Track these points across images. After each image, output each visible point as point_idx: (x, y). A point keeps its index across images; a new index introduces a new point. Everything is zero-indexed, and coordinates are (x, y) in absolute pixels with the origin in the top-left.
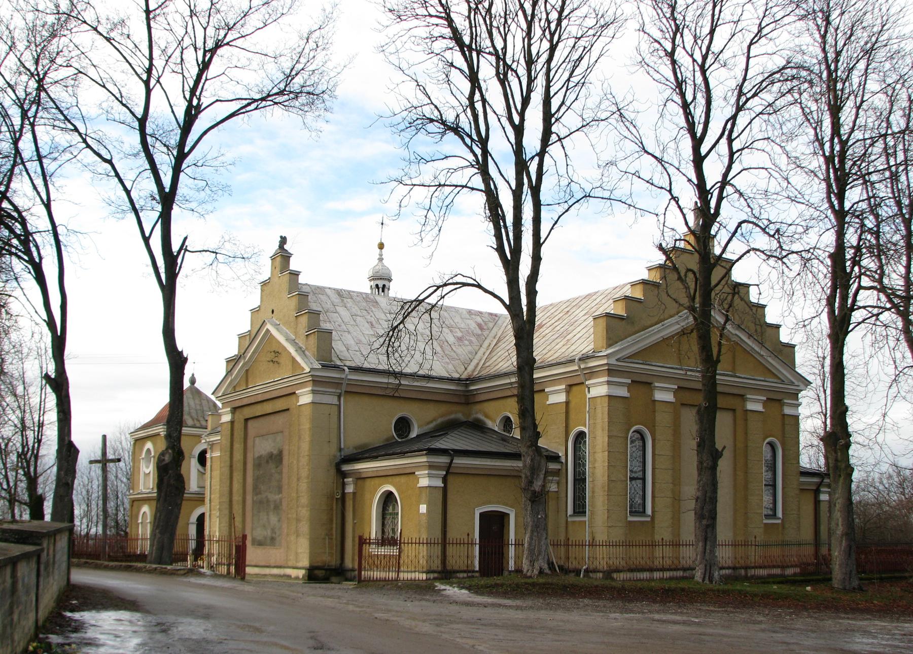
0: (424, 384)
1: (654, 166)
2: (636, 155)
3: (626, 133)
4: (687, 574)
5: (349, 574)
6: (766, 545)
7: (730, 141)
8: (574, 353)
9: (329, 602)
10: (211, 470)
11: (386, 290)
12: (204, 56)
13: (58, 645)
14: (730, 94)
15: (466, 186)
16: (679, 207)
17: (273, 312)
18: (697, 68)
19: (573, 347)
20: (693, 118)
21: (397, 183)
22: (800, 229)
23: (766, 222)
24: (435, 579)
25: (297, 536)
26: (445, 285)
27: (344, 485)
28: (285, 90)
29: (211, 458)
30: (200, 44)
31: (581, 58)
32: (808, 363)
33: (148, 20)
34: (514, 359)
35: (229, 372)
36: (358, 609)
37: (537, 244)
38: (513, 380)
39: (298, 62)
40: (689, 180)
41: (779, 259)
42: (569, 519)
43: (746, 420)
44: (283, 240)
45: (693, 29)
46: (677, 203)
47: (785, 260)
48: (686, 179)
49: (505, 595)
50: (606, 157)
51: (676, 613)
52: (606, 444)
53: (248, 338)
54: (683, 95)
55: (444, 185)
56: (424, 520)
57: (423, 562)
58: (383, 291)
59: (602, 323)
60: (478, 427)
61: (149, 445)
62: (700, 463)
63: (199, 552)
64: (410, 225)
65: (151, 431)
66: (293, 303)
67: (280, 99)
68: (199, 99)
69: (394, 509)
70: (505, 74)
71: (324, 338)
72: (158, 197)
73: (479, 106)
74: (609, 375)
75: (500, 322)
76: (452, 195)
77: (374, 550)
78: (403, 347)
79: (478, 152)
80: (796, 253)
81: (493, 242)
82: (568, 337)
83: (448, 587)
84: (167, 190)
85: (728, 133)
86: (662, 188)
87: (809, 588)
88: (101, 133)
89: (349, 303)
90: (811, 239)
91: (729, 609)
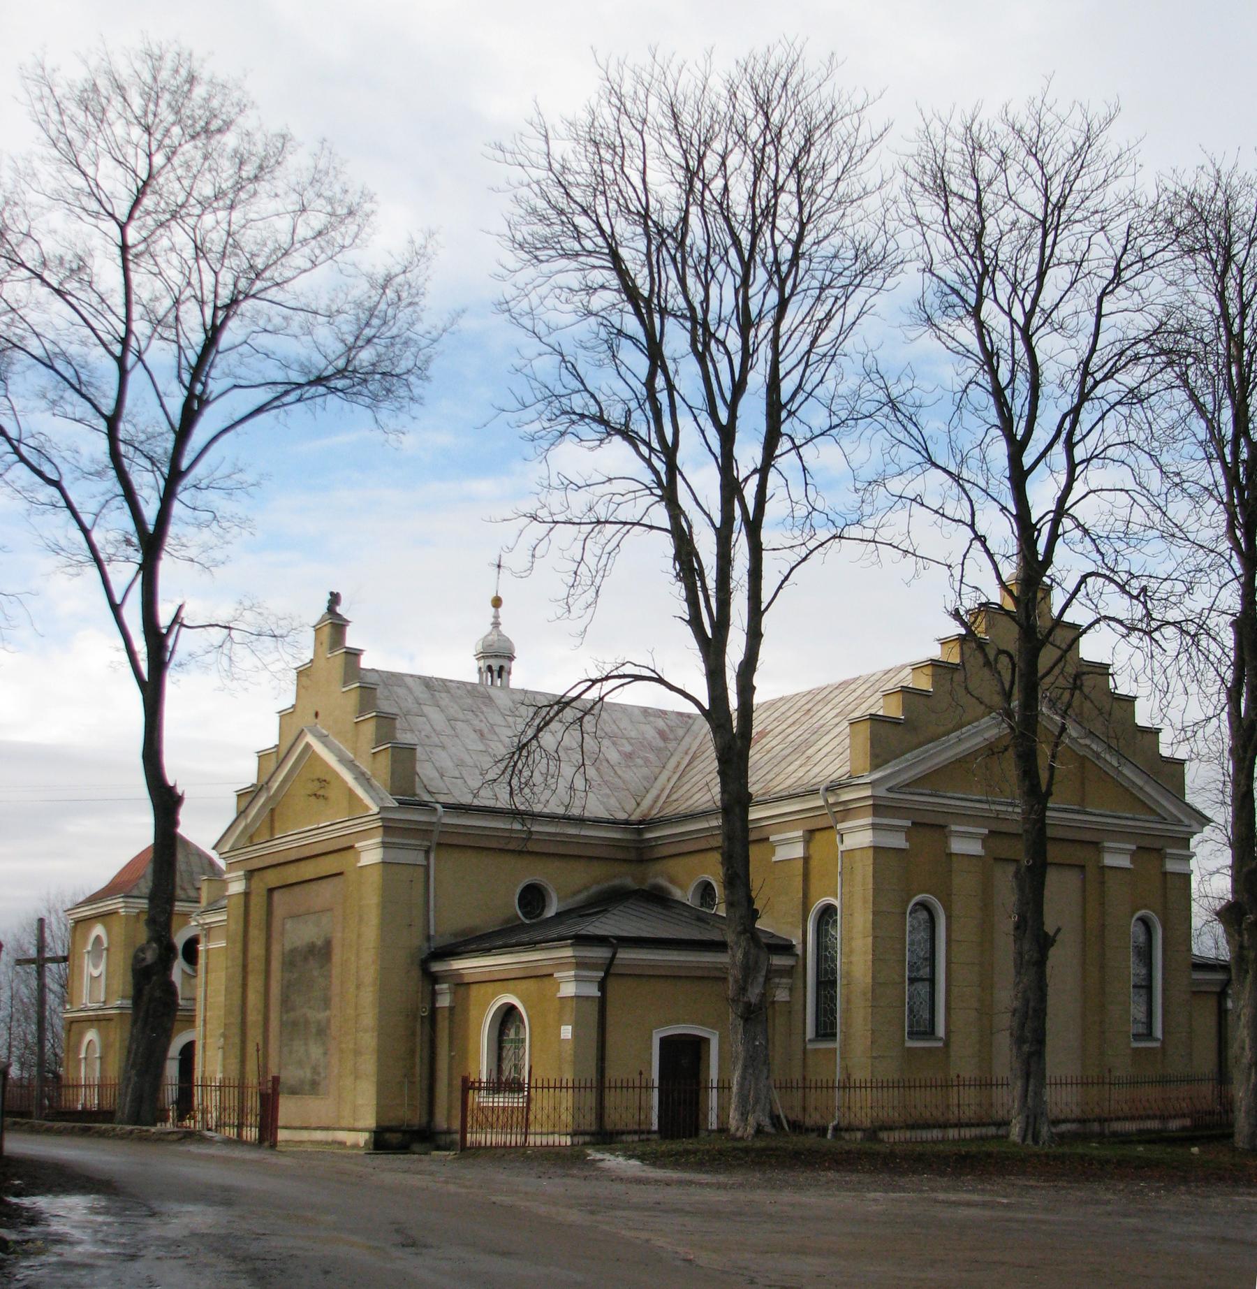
0: (572, 831)
1: (946, 486)
2: (918, 469)
3: (902, 435)
4: (1002, 1132)
5: (443, 1140)
6: (1133, 1083)
7: (1070, 446)
8: (818, 779)
9: (417, 1181)
10: (207, 972)
11: (504, 674)
12: (214, 316)
13: (17, 1242)
14: (1069, 376)
15: (638, 524)
16: (987, 551)
17: (317, 715)
18: (1018, 334)
19: (816, 770)
20: (1010, 410)
21: (528, 520)
22: (1180, 587)
23: (1125, 577)
24: (585, 1144)
25: (356, 1078)
26: (607, 678)
27: (434, 995)
28: (345, 369)
29: (207, 951)
30: (209, 297)
31: (829, 316)
32: (1213, 785)
33: (125, 260)
34: (717, 789)
35: (241, 813)
36: (464, 1190)
37: (756, 612)
38: (714, 823)
39: (367, 324)
40: (1003, 508)
41: (1145, 633)
42: (809, 1046)
43: (1103, 883)
44: (335, 599)
45: (1010, 273)
46: (984, 544)
47: (1156, 635)
48: (998, 507)
49: (700, 1166)
50: (868, 474)
51: (973, 1191)
52: (869, 925)
53: (274, 756)
54: (994, 373)
55: (607, 522)
56: (568, 1050)
57: (566, 1117)
58: (500, 676)
59: (865, 729)
60: (658, 898)
61: (98, 930)
62: (1020, 954)
63: (185, 1103)
64: (552, 576)
65: (103, 907)
66: (352, 701)
67: (340, 384)
68: (205, 385)
69: (517, 1033)
70: (706, 346)
71: (403, 759)
72: (135, 540)
73: (663, 397)
74: (875, 815)
75: (695, 728)
76: (619, 535)
77: (482, 1099)
78: (538, 778)
79: (661, 467)
80: (1173, 624)
81: (683, 609)
82: (810, 752)
83: (607, 1156)
84: (151, 528)
85: (1067, 436)
86: (960, 521)
87: (1195, 1150)
88: (42, 438)
89: (444, 699)
90: (1199, 601)
91: (1060, 1184)
